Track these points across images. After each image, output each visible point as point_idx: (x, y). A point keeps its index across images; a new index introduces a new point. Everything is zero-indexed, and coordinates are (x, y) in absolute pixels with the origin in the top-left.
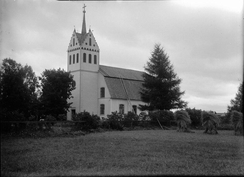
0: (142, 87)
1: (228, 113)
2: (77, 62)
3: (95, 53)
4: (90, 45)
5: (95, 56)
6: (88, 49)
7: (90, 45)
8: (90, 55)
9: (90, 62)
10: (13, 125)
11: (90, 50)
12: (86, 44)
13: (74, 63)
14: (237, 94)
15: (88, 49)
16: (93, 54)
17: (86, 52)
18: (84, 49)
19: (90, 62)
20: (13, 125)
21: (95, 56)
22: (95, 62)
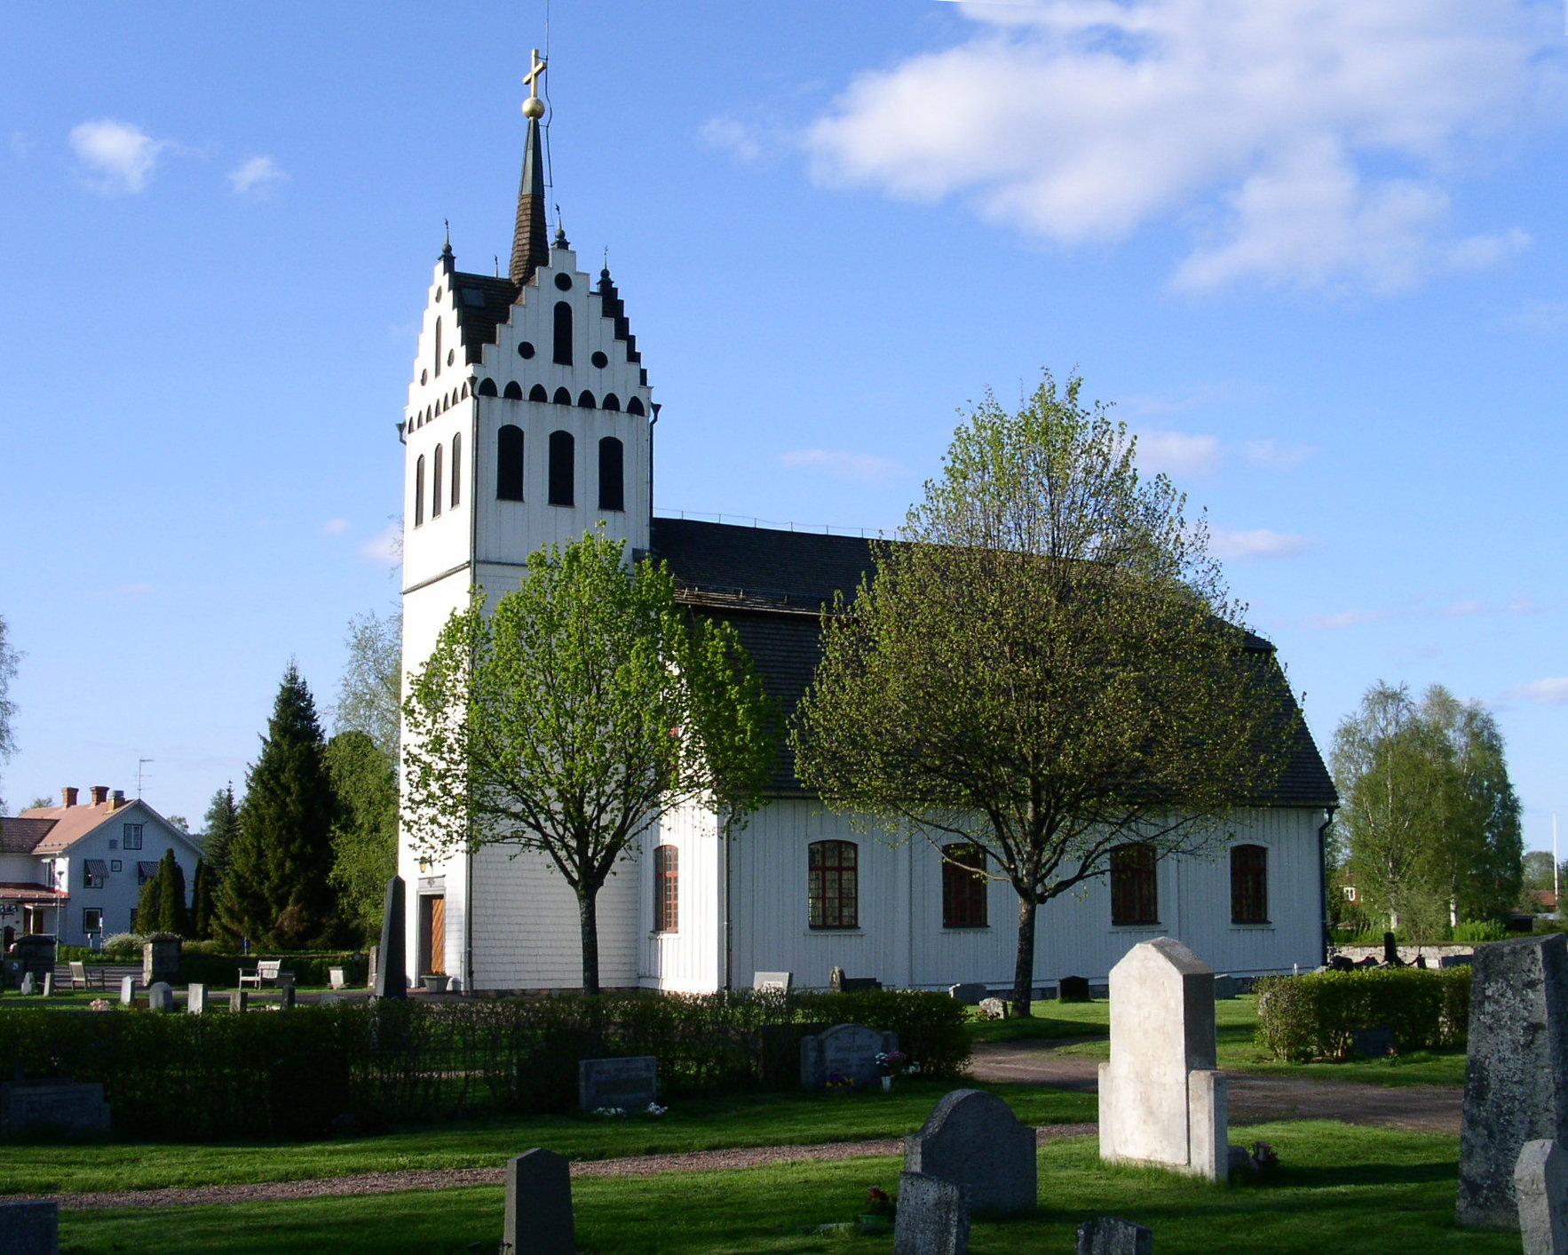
0: (318, 723)
1: (332, 1011)
2: (455, 501)
3: (621, 427)
4: (563, 354)
5: (611, 452)
6: (538, 394)
7: (563, 354)
8: (561, 446)
9: (561, 493)
10: (228, 1071)
11: (562, 397)
12: (600, 360)
13: (437, 510)
14: (230, 798)
15: (587, 400)
16: (588, 433)
17: (571, 420)
18: (599, 403)
19: (561, 493)
20: (228, 1071)
21: (611, 452)
22: (611, 497)
